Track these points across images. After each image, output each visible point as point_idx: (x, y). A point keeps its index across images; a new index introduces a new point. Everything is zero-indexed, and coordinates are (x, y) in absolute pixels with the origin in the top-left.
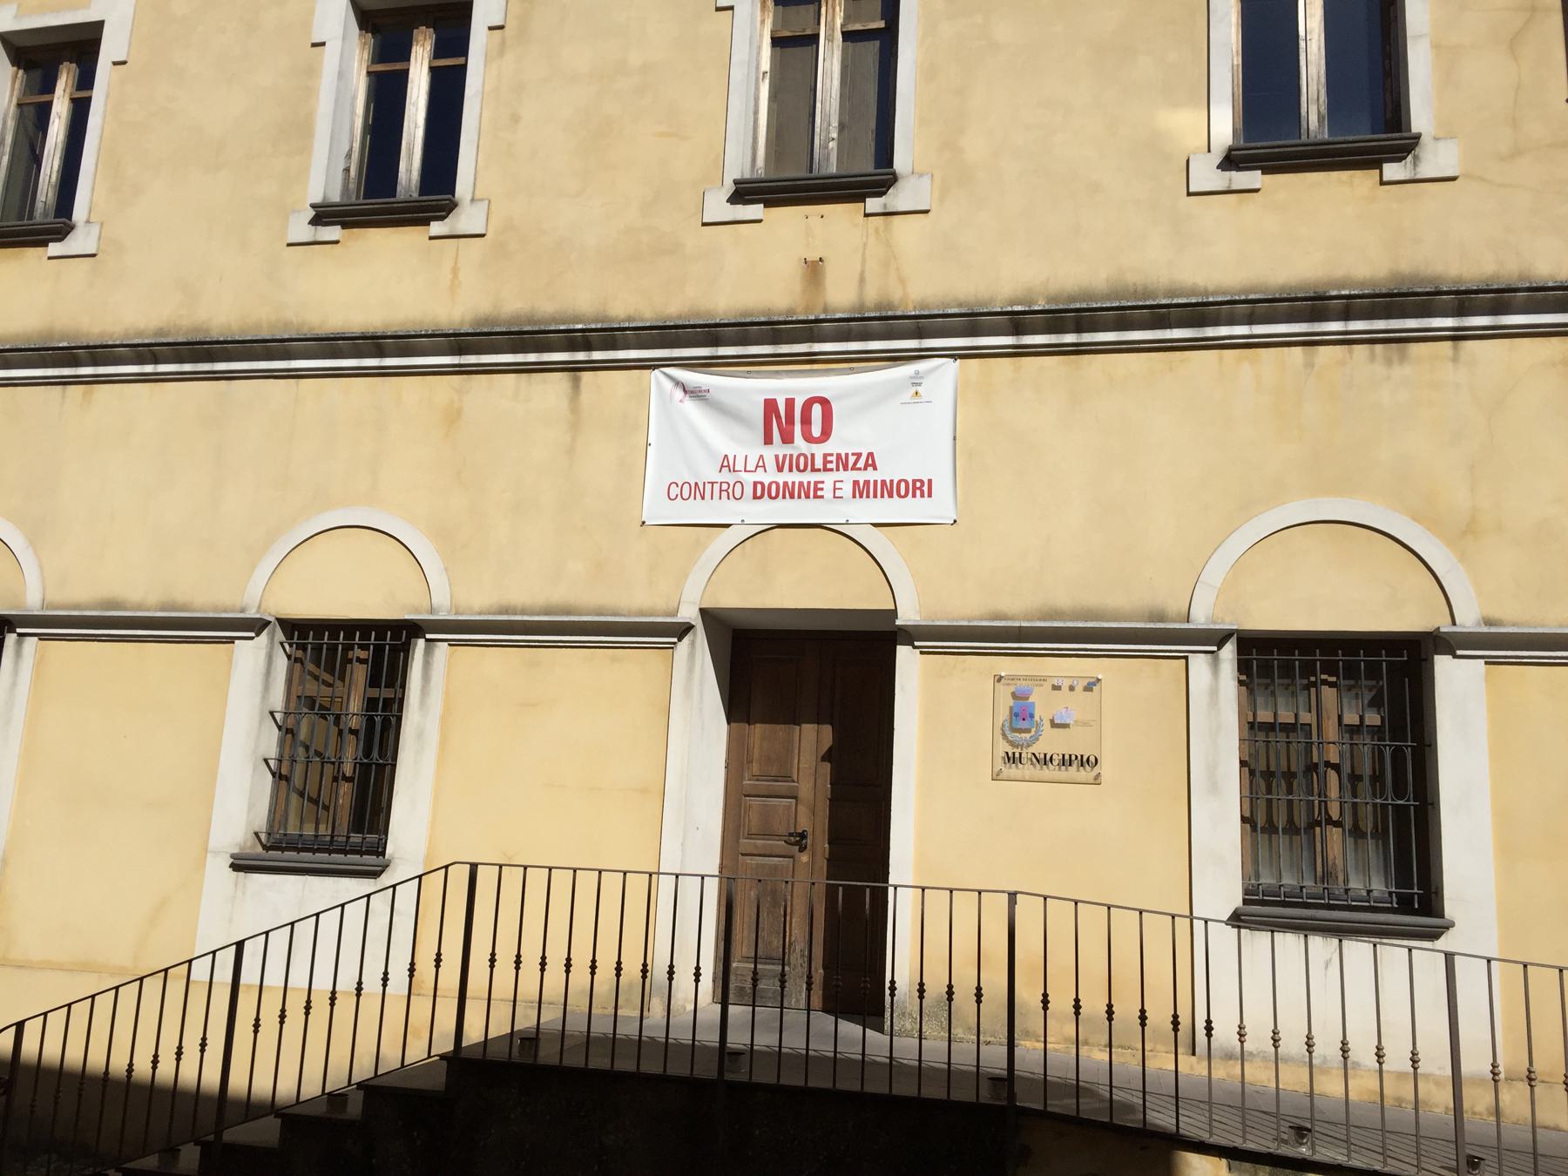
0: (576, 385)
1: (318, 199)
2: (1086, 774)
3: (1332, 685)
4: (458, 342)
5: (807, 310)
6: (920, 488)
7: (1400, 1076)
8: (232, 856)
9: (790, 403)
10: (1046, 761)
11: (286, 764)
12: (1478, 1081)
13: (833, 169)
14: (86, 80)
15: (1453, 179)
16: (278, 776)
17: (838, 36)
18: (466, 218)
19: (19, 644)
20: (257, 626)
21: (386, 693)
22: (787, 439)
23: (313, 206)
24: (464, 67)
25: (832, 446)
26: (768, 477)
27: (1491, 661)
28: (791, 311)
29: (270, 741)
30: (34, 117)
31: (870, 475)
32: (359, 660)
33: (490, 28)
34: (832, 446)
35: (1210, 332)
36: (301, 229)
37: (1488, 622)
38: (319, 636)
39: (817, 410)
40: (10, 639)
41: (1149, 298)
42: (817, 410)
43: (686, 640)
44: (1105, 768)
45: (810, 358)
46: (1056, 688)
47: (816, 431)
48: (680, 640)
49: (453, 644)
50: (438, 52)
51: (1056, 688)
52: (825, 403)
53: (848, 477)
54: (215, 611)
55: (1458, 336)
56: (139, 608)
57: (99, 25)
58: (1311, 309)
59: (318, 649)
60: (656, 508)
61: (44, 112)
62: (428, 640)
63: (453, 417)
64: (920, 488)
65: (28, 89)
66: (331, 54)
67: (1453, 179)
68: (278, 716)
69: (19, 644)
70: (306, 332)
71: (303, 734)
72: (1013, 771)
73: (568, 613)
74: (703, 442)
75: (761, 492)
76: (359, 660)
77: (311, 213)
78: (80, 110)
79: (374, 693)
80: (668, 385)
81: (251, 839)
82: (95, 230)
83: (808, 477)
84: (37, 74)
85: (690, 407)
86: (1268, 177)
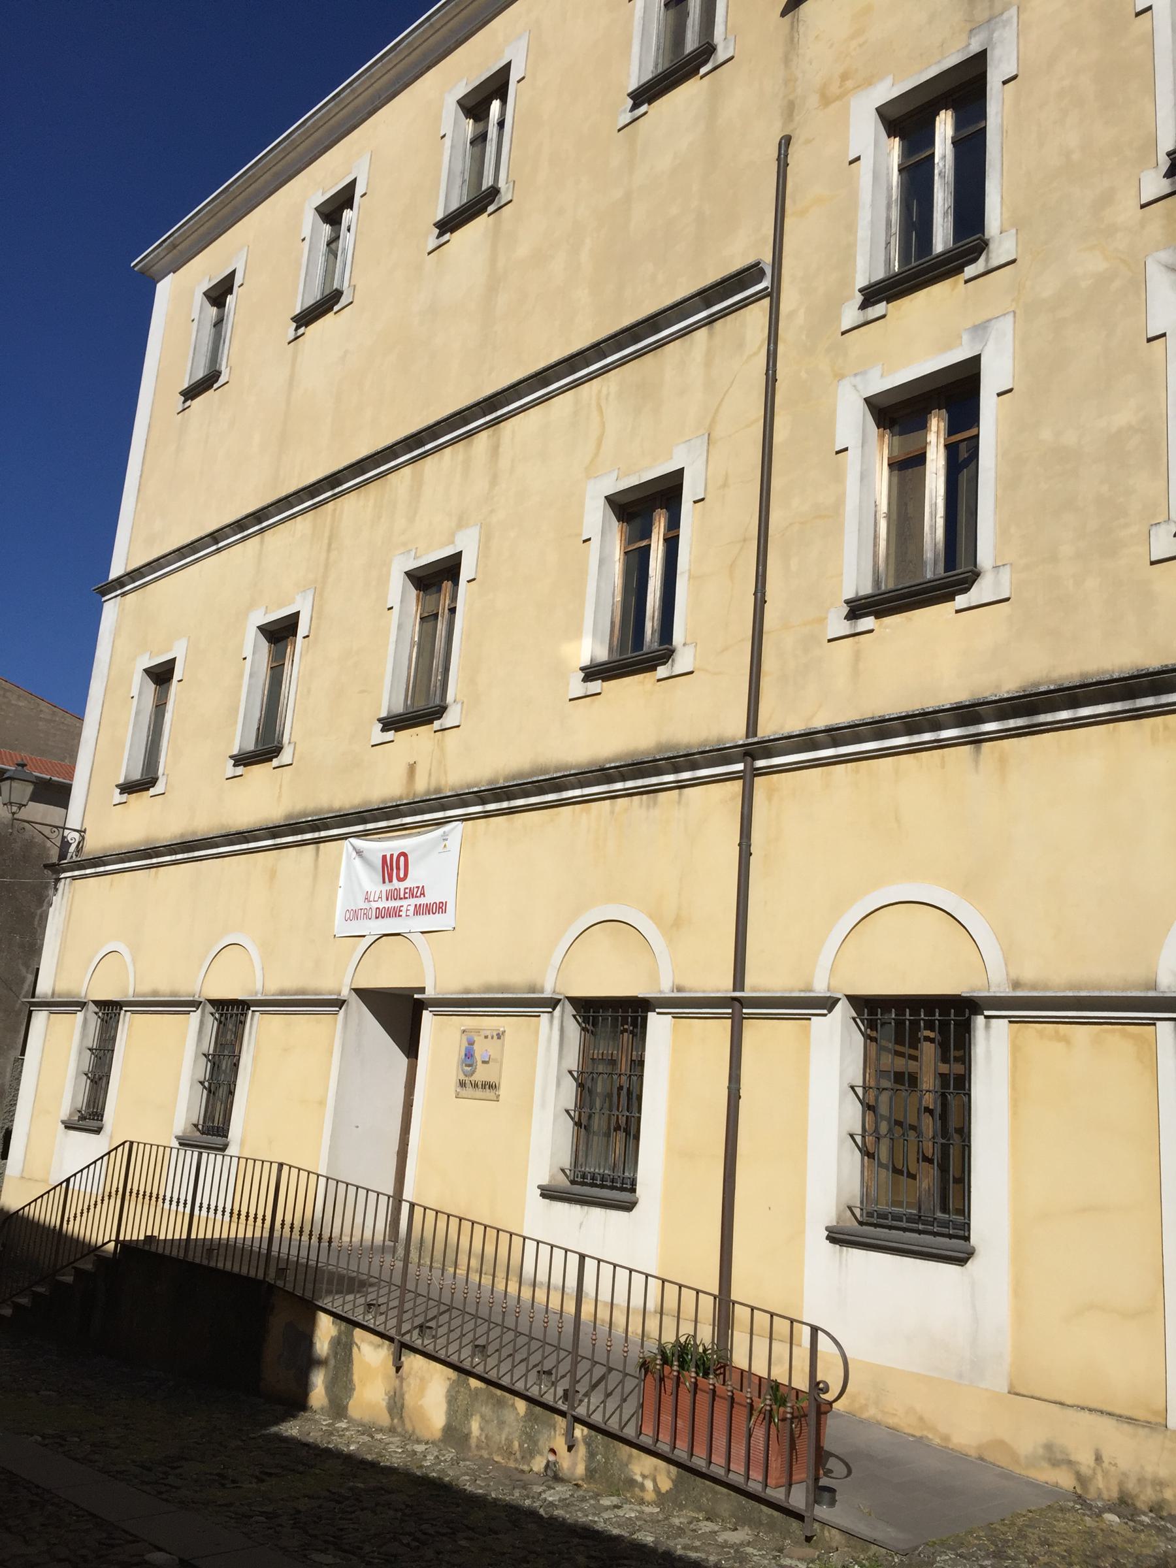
0: (318, 849)
1: (850, 595)
2: (489, 1094)
3: (932, 1040)
4: (274, 831)
5: (408, 795)
6: (441, 907)
7: (605, 1303)
8: (827, 1229)
9: (392, 856)
10: (476, 1085)
11: (870, 1140)
12: (556, 1289)
13: (891, 586)
14: (674, 523)
15: (692, 673)
16: (866, 1153)
17: (446, 611)
18: (683, 661)
19: (987, 1027)
20: (196, 1004)
21: (958, 1069)
22: (391, 881)
23: (582, 669)
24: (649, 546)
25: (408, 883)
26: (383, 904)
27: (676, 1017)
28: (401, 798)
29: (853, 1115)
30: (637, 564)
31: (422, 901)
32: (927, 1039)
33: (999, 395)
34: (408, 883)
35: (196, 854)
36: (577, 687)
37: (679, 990)
38: (900, 1012)
39: (402, 858)
40: (980, 1020)
41: (571, 769)
42: (402, 858)
43: (558, 1009)
44: (502, 1092)
45: (403, 827)
46: (486, 1037)
47: (402, 875)
48: (830, 1011)
49: (133, 1012)
50: (952, 430)
51: (486, 1037)
52: (404, 854)
53: (413, 901)
54: (1117, 989)
55: (680, 786)
56: (1034, 988)
57: (681, 471)
58: (967, 719)
59: (900, 1024)
60: (341, 927)
61: (645, 552)
62: (987, 1017)
63: (273, 874)
64: (441, 907)
65: (630, 540)
66: (853, 458)
67: (692, 673)
68: (575, 1074)
69: (987, 1027)
70: (233, 830)
71: (883, 1109)
72: (464, 1092)
73: (303, 993)
74: (360, 885)
75: (381, 914)
76: (927, 1039)
77: (845, 609)
78: (672, 545)
79: (944, 1068)
80: (350, 848)
81: (190, 1128)
82: (459, 706)
83: (397, 903)
84: (638, 522)
85: (358, 862)
86: (605, 684)
